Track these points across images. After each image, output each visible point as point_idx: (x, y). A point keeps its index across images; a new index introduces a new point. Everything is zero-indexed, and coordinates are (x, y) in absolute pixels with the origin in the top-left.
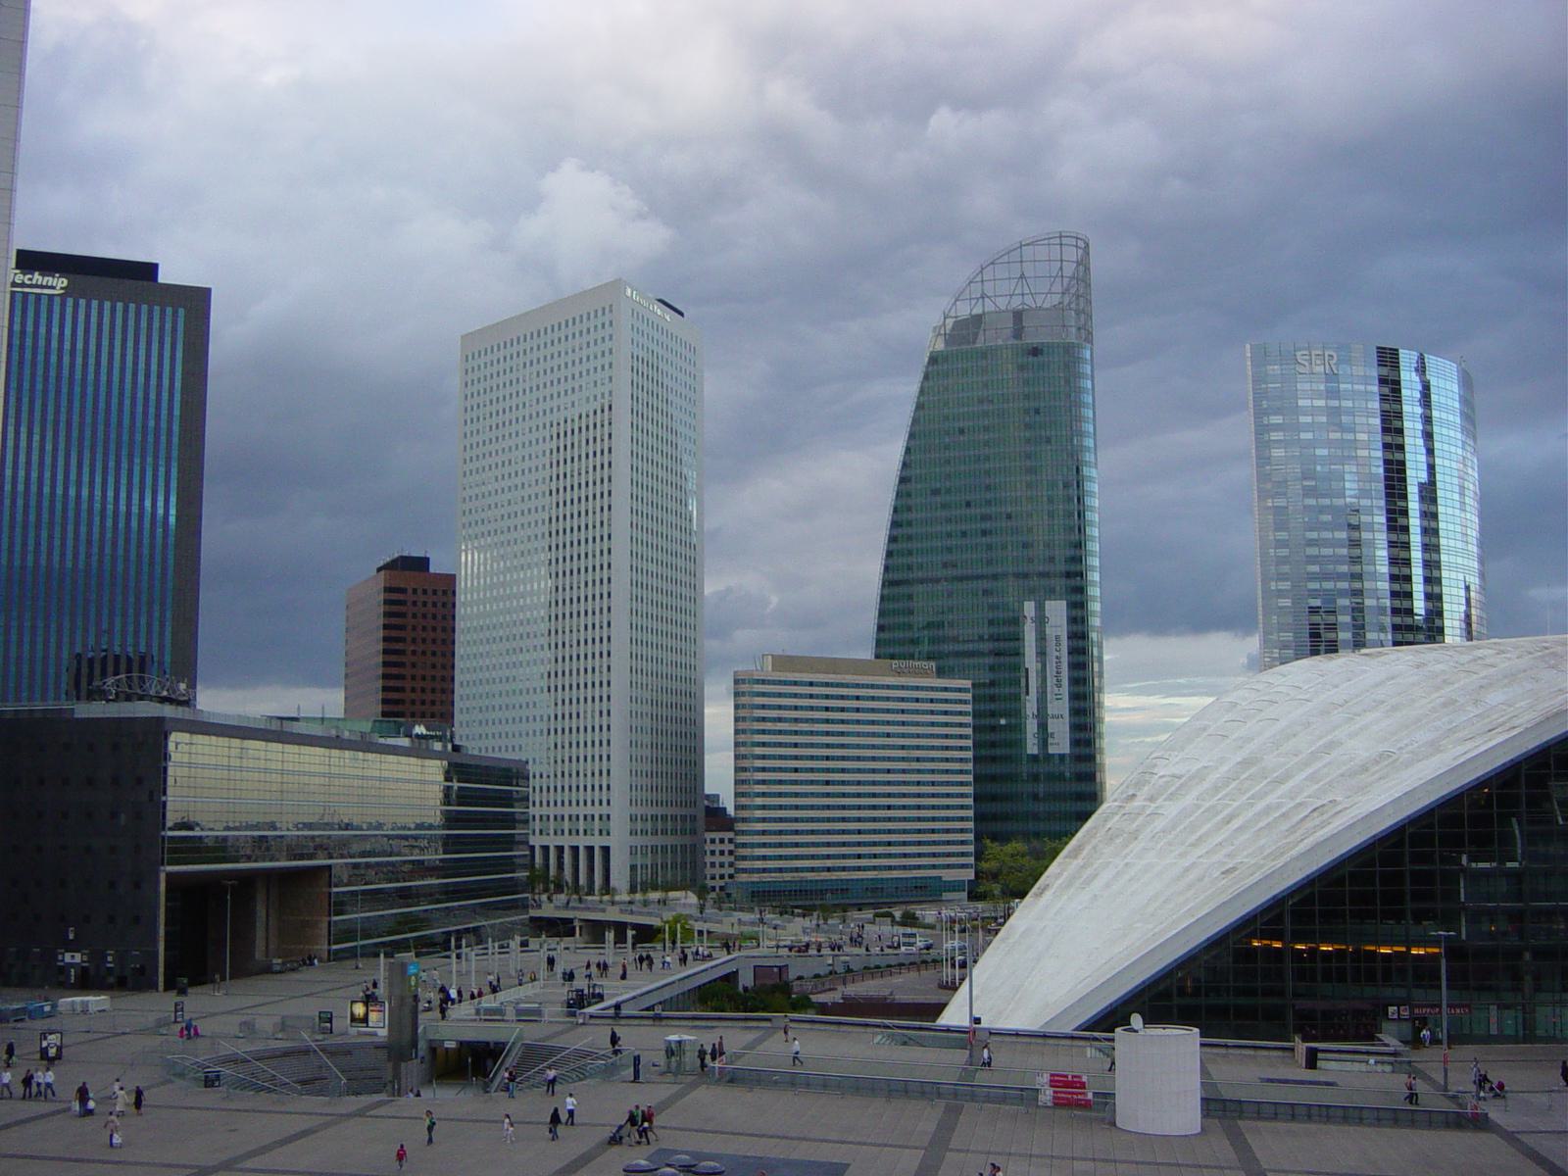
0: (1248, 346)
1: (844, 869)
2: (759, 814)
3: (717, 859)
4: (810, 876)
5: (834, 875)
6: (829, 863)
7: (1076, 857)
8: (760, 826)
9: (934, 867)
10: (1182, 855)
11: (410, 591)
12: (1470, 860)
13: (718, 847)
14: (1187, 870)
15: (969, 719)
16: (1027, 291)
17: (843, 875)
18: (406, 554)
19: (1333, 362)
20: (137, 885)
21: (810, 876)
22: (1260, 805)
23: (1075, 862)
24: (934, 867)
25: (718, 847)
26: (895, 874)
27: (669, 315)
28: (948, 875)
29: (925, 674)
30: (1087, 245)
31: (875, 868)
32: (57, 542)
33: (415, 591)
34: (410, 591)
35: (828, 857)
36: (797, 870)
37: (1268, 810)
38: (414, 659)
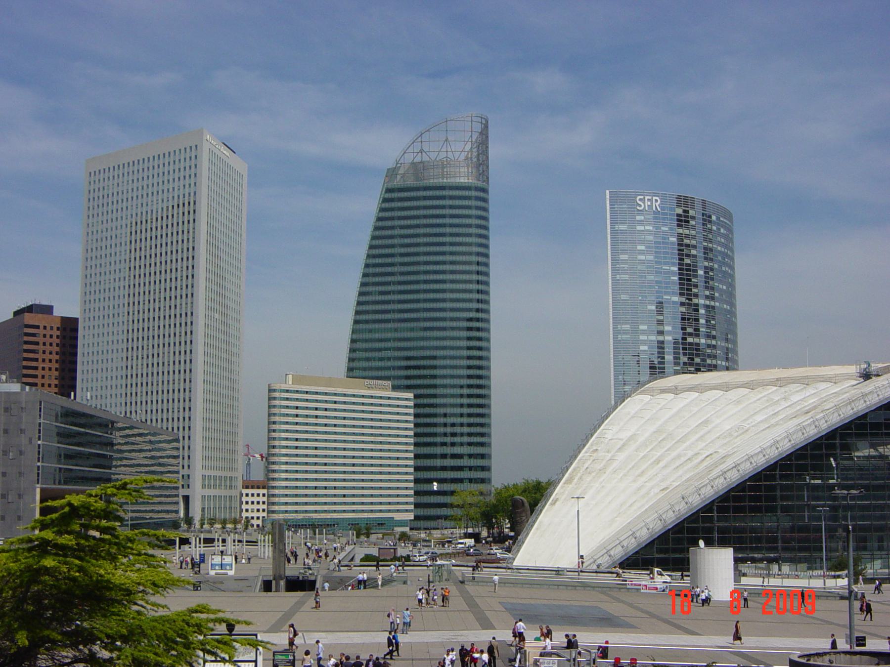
0: (608, 192)
1: (335, 511)
2: (284, 475)
3: (250, 507)
4: (314, 516)
5: (329, 516)
6: (326, 508)
7: (571, 483)
8: (284, 484)
9: (389, 511)
10: (634, 481)
11: (42, 327)
12: (810, 480)
13: (250, 499)
14: (639, 489)
15: (411, 418)
16: (449, 149)
17: (335, 515)
18: (37, 302)
19: (657, 204)
20: (20, 496)
21: (314, 516)
22: (674, 454)
23: (571, 486)
24: (389, 511)
25: (250, 499)
26: (366, 515)
27: (227, 152)
28: (398, 517)
29: (384, 388)
30: (487, 122)
31: (354, 511)
32: (377, 279)
33: (45, 328)
34: (42, 327)
35: (326, 504)
36: (306, 512)
37: (679, 456)
38: (43, 373)
